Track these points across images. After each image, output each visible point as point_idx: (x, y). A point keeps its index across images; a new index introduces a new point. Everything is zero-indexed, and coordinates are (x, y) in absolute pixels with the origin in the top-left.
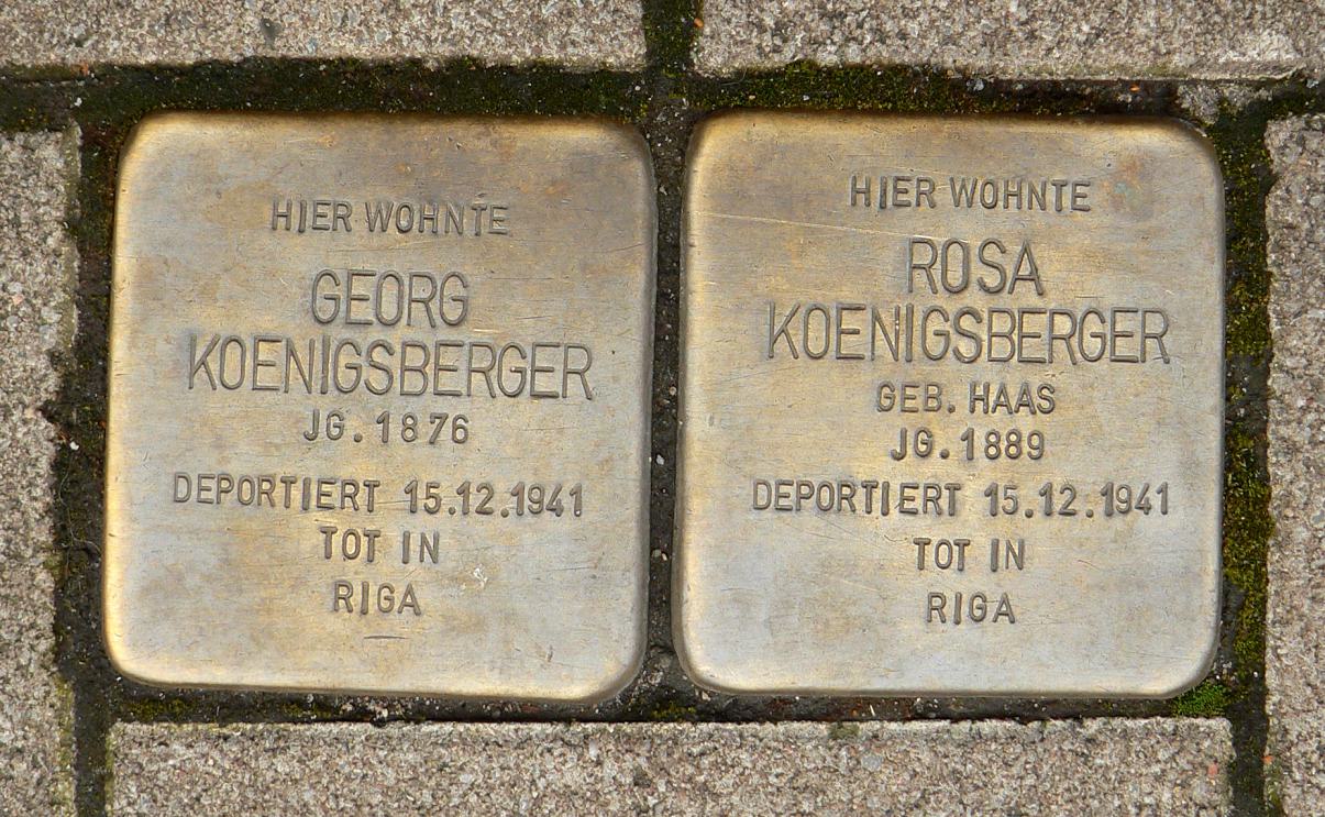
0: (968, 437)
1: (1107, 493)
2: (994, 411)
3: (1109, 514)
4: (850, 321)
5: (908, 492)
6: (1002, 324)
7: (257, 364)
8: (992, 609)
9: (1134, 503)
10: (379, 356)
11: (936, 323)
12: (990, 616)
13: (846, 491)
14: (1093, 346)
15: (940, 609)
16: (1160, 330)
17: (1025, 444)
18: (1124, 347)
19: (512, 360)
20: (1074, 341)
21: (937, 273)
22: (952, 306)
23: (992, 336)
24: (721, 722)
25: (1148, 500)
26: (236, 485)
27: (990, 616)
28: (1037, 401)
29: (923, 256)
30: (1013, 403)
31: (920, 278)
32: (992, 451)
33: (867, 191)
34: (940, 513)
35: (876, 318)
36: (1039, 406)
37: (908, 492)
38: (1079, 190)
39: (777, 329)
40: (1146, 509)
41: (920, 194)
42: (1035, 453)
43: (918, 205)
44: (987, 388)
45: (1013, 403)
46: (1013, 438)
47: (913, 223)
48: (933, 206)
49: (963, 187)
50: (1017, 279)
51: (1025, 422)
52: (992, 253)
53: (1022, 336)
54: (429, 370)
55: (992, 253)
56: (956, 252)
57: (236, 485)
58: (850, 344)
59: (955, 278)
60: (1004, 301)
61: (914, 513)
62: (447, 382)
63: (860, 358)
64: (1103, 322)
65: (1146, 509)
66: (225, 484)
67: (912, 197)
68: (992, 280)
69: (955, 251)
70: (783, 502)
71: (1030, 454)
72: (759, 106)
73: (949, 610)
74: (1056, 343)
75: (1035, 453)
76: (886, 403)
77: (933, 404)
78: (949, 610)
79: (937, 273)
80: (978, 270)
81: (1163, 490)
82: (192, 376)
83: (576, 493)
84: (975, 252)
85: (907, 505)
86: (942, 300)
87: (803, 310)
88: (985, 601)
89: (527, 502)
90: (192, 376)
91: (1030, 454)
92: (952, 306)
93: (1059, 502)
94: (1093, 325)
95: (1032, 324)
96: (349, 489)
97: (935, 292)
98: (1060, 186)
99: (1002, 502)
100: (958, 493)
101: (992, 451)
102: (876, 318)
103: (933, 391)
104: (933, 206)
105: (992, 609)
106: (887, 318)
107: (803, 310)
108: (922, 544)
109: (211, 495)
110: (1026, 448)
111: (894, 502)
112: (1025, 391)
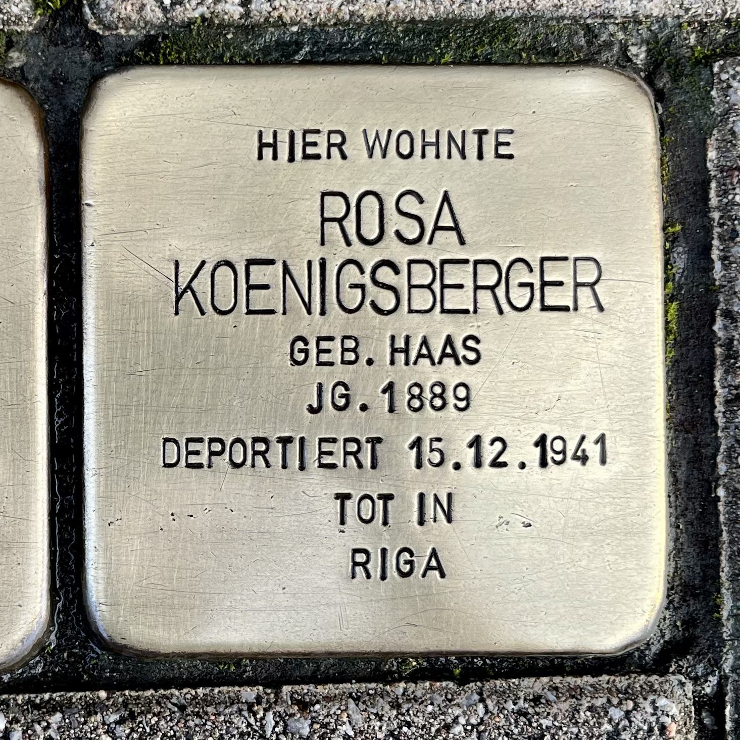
0: (390, 388)
1: (541, 442)
2: (415, 363)
3: (543, 464)
4: (259, 274)
5: (326, 447)
6: (422, 275)
7: (250, 287)
8: (421, 565)
9: (570, 454)
10: (385, 275)
11: (351, 274)
12: (420, 569)
13: (261, 447)
14: (520, 297)
15: (364, 565)
16: (592, 279)
17: (428, 395)
18: (553, 297)
19: (520, 275)
20: (501, 292)
21: (350, 225)
22: (369, 257)
23: (411, 286)
24: (725, 720)
25: (584, 451)
26: (228, 449)
27: (420, 569)
28: (461, 352)
29: (336, 207)
30: (437, 356)
31: (333, 229)
32: (416, 403)
33: (274, 146)
34: (360, 465)
35: (286, 270)
36: (464, 357)
37: (326, 447)
38: (502, 138)
39: (183, 284)
40: (584, 459)
41: (330, 145)
42: (462, 404)
43: (329, 157)
44: (407, 339)
45: (437, 356)
46: (438, 390)
47: (327, 174)
48: (344, 157)
49: (377, 136)
50: (437, 228)
51: (450, 374)
52: (410, 204)
53: (444, 286)
54: (437, 287)
55: (410, 204)
56: (370, 205)
57: (228, 449)
58: (259, 299)
59: (371, 232)
60: (422, 251)
61: (199, 466)
62: (453, 300)
63: (272, 312)
64: (531, 271)
65: (584, 459)
66: (217, 447)
67: (322, 150)
68: (412, 232)
69: (370, 203)
70: (193, 459)
71: (456, 407)
72: (139, 59)
73: (375, 567)
74: (481, 294)
75: (462, 404)
76: (300, 357)
77: (351, 356)
78: (375, 567)
79: (350, 225)
80: (395, 222)
81: (601, 440)
82: (178, 299)
83: (601, 440)
84: (390, 205)
85: (327, 460)
86: (359, 251)
87: (208, 268)
88: (412, 555)
89: (550, 454)
90: (178, 299)
91: (456, 407)
92: (369, 257)
93: (489, 452)
94: (520, 275)
95: (453, 275)
96: (353, 447)
97: (348, 243)
98: (481, 133)
99: (427, 454)
100: (378, 446)
101: (416, 403)
102: (286, 270)
103: (351, 344)
104: (344, 157)
105: (421, 565)
106: (300, 272)
107: (208, 268)
108: (343, 498)
109: (203, 459)
110: (452, 401)
111: (312, 454)
112: (449, 341)
